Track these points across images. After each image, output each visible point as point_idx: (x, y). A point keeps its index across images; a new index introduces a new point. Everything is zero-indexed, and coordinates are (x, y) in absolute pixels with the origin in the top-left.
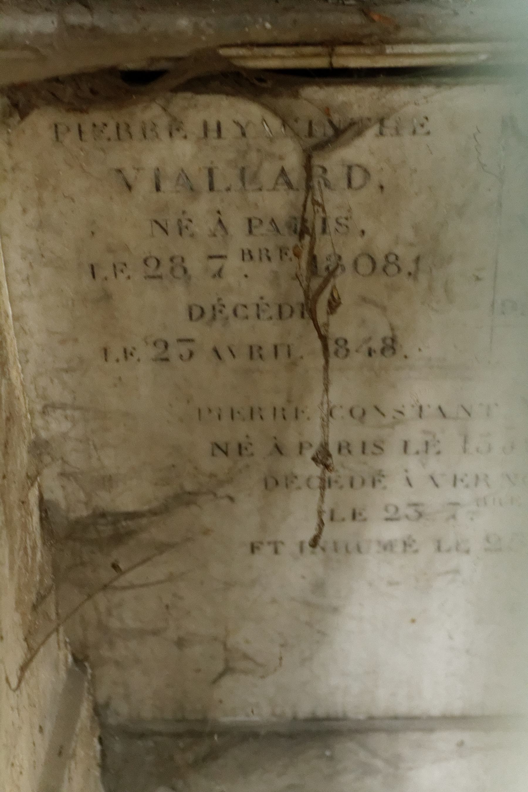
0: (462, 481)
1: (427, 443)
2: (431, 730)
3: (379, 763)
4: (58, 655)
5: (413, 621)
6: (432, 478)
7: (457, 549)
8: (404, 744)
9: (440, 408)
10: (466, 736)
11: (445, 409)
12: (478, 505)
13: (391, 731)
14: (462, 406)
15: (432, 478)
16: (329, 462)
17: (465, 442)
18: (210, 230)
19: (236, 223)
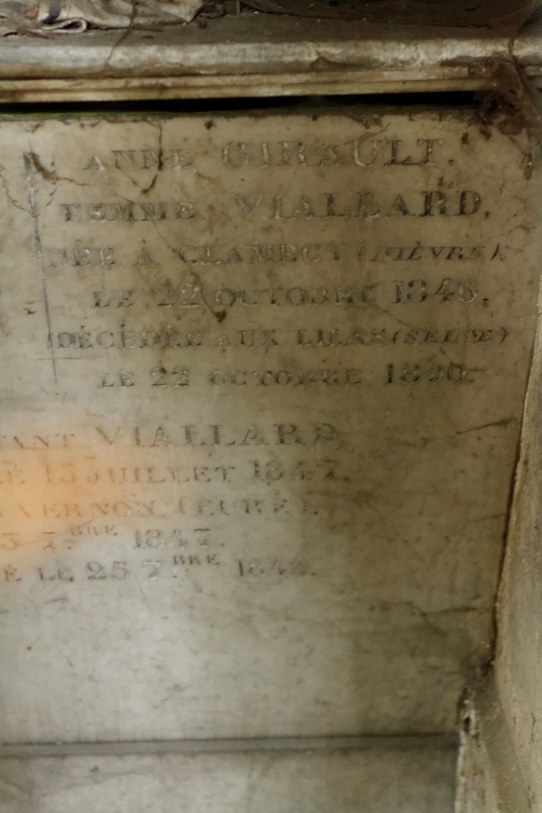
0: (52, 510)
1: (9, 472)
2: (63, 756)
3: (14, 790)
4: (169, 304)
5: (29, 648)
6: (22, 508)
7: (60, 578)
8: (38, 770)
9: (15, 438)
10: (99, 762)
11: (22, 439)
12: (73, 534)
13: (23, 758)
14: (38, 437)
15: (22, 508)
16: (338, 164)
17: (48, 471)
18: (469, 125)
19: (51, 213)
